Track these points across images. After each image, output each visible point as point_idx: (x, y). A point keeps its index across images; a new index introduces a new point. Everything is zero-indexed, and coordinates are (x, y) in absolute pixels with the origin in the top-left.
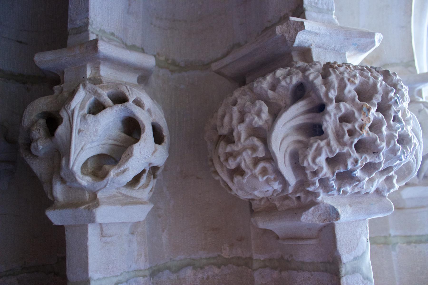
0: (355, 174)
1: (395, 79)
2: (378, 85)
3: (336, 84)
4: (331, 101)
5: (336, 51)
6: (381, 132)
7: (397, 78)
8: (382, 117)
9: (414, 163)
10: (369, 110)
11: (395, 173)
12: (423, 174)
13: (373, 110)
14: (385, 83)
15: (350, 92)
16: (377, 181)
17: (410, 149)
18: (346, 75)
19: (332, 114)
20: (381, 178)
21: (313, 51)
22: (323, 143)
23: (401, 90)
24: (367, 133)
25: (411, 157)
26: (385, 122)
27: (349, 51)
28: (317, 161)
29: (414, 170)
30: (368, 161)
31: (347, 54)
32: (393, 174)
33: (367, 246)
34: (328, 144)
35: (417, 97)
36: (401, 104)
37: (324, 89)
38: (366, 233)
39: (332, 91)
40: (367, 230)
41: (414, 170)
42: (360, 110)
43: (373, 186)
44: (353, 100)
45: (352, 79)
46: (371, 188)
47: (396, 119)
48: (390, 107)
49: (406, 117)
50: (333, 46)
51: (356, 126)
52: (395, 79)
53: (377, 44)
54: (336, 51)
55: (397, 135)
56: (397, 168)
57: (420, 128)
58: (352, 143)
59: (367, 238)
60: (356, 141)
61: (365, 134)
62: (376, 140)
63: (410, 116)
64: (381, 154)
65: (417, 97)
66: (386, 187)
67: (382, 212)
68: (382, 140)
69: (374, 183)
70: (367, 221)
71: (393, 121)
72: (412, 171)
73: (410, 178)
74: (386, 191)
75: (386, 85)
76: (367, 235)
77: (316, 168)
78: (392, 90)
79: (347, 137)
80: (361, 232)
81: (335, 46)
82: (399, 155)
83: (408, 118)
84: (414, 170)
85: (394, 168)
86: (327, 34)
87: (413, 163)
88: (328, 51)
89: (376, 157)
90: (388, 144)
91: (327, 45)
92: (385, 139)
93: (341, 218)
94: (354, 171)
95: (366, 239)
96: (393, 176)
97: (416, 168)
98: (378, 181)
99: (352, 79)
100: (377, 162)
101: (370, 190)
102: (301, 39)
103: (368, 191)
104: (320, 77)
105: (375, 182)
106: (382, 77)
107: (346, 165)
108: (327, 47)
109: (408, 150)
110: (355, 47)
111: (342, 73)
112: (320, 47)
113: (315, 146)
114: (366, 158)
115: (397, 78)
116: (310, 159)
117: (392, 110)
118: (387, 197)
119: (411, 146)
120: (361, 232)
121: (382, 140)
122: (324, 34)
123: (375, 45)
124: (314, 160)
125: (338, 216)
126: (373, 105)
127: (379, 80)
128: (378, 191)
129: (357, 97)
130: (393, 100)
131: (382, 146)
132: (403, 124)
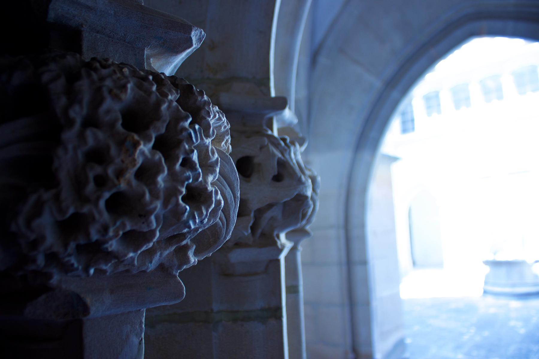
0: (107, 249)
1: (201, 100)
2: (164, 107)
3: (86, 97)
4: (71, 123)
5: (128, 43)
6: (155, 183)
7: (203, 100)
8: (160, 159)
9: (223, 227)
10: (136, 145)
11: (193, 240)
12: (259, 231)
13: (145, 148)
14: (176, 105)
15: (108, 111)
16: (158, 254)
17: (207, 211)
18: (108, 83)
19: (70, 147)
20: (166, 250)
21: (84, 35)
22: (47, 195)
23: (206, 118)
24: (129, 183)
25: (213, 220)
26: (164, 168)
27: (149, 47)
28: (36, 223)
29: (223, 237)
30: (128, 228)
31: (147, 52)
32: (187, 243)
33: (139, 350)
34: (57, 198)
35: (265, 127)
36: (199, 141)
37: (63, 101)
38: (139, 330)
39: (77, 108)
40: (141, 327)
41: (222, 237)
42: (121, 143)
43: (151, 262)
44: (112, 125)
45: (116, 91)
46: (147, 264)
47: (187, 163)
48: (179, 143)
49: (209, 161)
50: (121, 34)
51: (110, 171)
52: (201, 100)
53: (195, 45)
54: (128, 43)
55: (184, 190)
56: (192, 235)
57: (237, 176)
58: (98, 198)
59: (140, 339)
60: (107, 195)
61: (123, 186)
62: (143, 195)
63: (217, 159)
64: (153, 218)
65: (265, 127)
66: (176, 262)
67: (166, 300)
68: (155, 195)
69: (154, 257)
70: (143, 313)
71: (182, 165)
72: (219, 238)
73: (217, 248)
74: (176, 267)
75: (178, 108)
76: (141, 333)
77: (33, 237)
78: (186, 119)
79: (91, 187)
80: (131, 331)
81: (125, 35)
82: (184, 220)
83: (212, 162)
84: (222, 237)
85: (187, 235)
86: (109, 12)
87: (222, 226)
88: (113, 41)
89: (143, 223)
90: (165, 204)
91: (110, 30)
92: (162, 195)
93: (92, 312)
94: (106, 242)
95: (139, 339)
96: (188, 245)
97: (225, 235)
98: (161, 254)
99: (116, 91)
100: (146, 230)
101: (146, 267)
102: (60, 10)
103: (144, 269)
104: (62, 81)
105: (156, 256)
106: (176, 95)
107: (88, 235)
108: (111, 34)
109: (202, 213)
110: (160, 42)
111: (102, 79)
112: (98, 32)
113: (33, 198)
114: (123, 225)
115: (203, 100)
116: (21, 221)
117: (182, 148)
118: (177, 276)
119: (209, 206)
120: (131, 331)
121: (155, 195)
122: (104, 11)
123: (192, 45)
124: (29, 222)
125: (86, 310)
126: (147, 139)
127: (168, 99)
128: (161, 267)
129: (120, 122)
130: (184, 134)
131: (153, 206)
132: (198, 172)
